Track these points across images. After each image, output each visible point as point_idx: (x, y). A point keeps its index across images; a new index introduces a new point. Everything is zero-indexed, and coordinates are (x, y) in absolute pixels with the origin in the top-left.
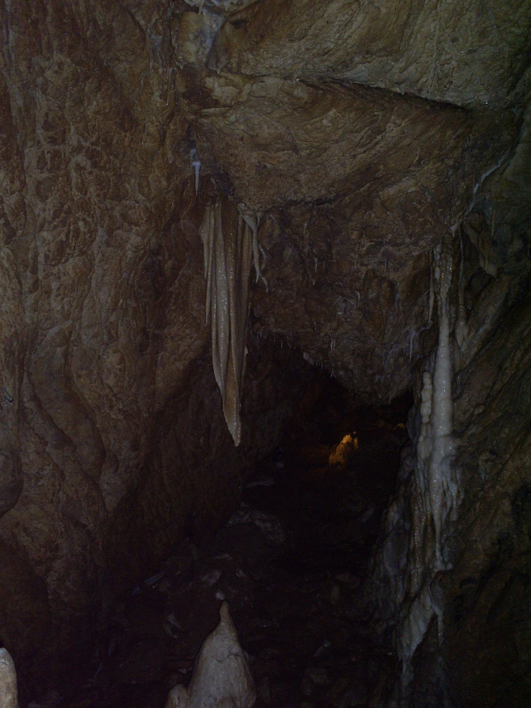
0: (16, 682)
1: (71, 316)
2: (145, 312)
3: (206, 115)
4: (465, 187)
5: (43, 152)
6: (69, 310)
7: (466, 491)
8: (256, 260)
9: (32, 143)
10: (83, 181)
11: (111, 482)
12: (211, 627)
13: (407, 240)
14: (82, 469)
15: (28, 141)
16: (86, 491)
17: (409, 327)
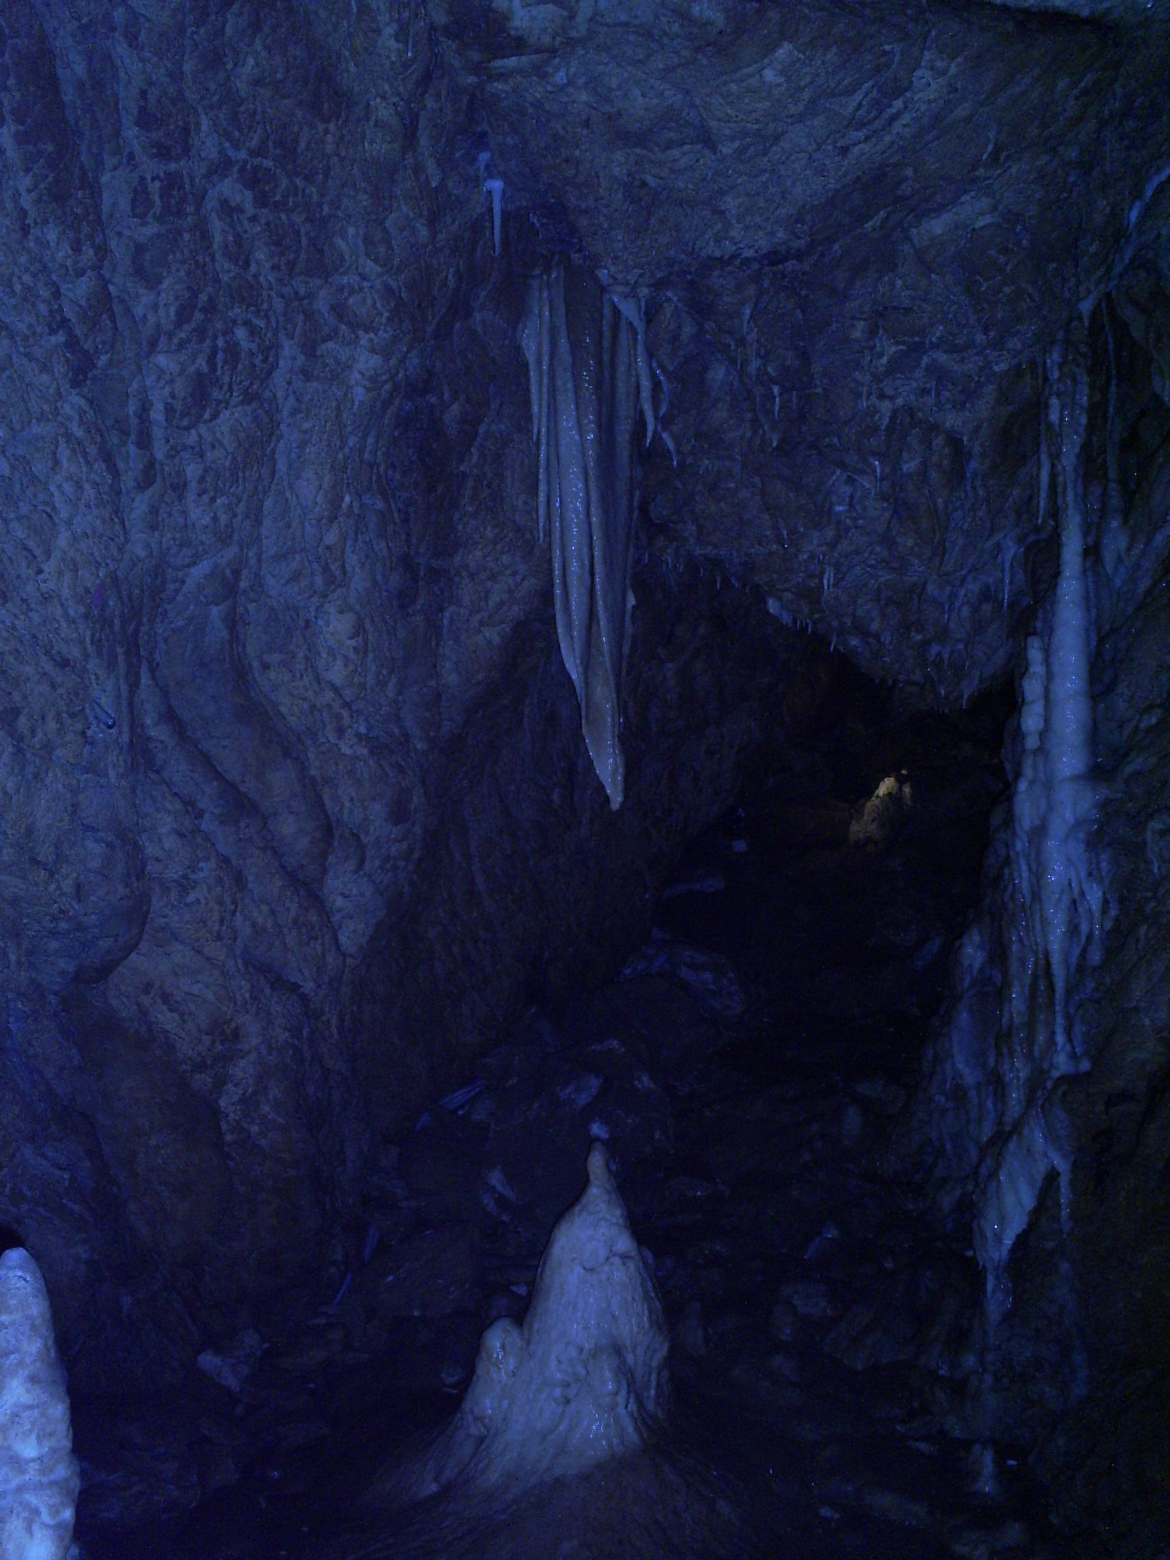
0: (48, 1316)
1: (236, 537)
2: (406, 520)
3: (502, 75)
4: (1108, 209)
5: (143, 179)
6: (230, 524)
7: (1121, 900)
8: (646, 394)
9: (115, 160)
10: (238, 237)
11: (352, 894)
12: (570, 1195)
13: (980, 338)
14: (283, 867)
15: (106, 157)
16: (293, 914)
17: (1002, 535)
